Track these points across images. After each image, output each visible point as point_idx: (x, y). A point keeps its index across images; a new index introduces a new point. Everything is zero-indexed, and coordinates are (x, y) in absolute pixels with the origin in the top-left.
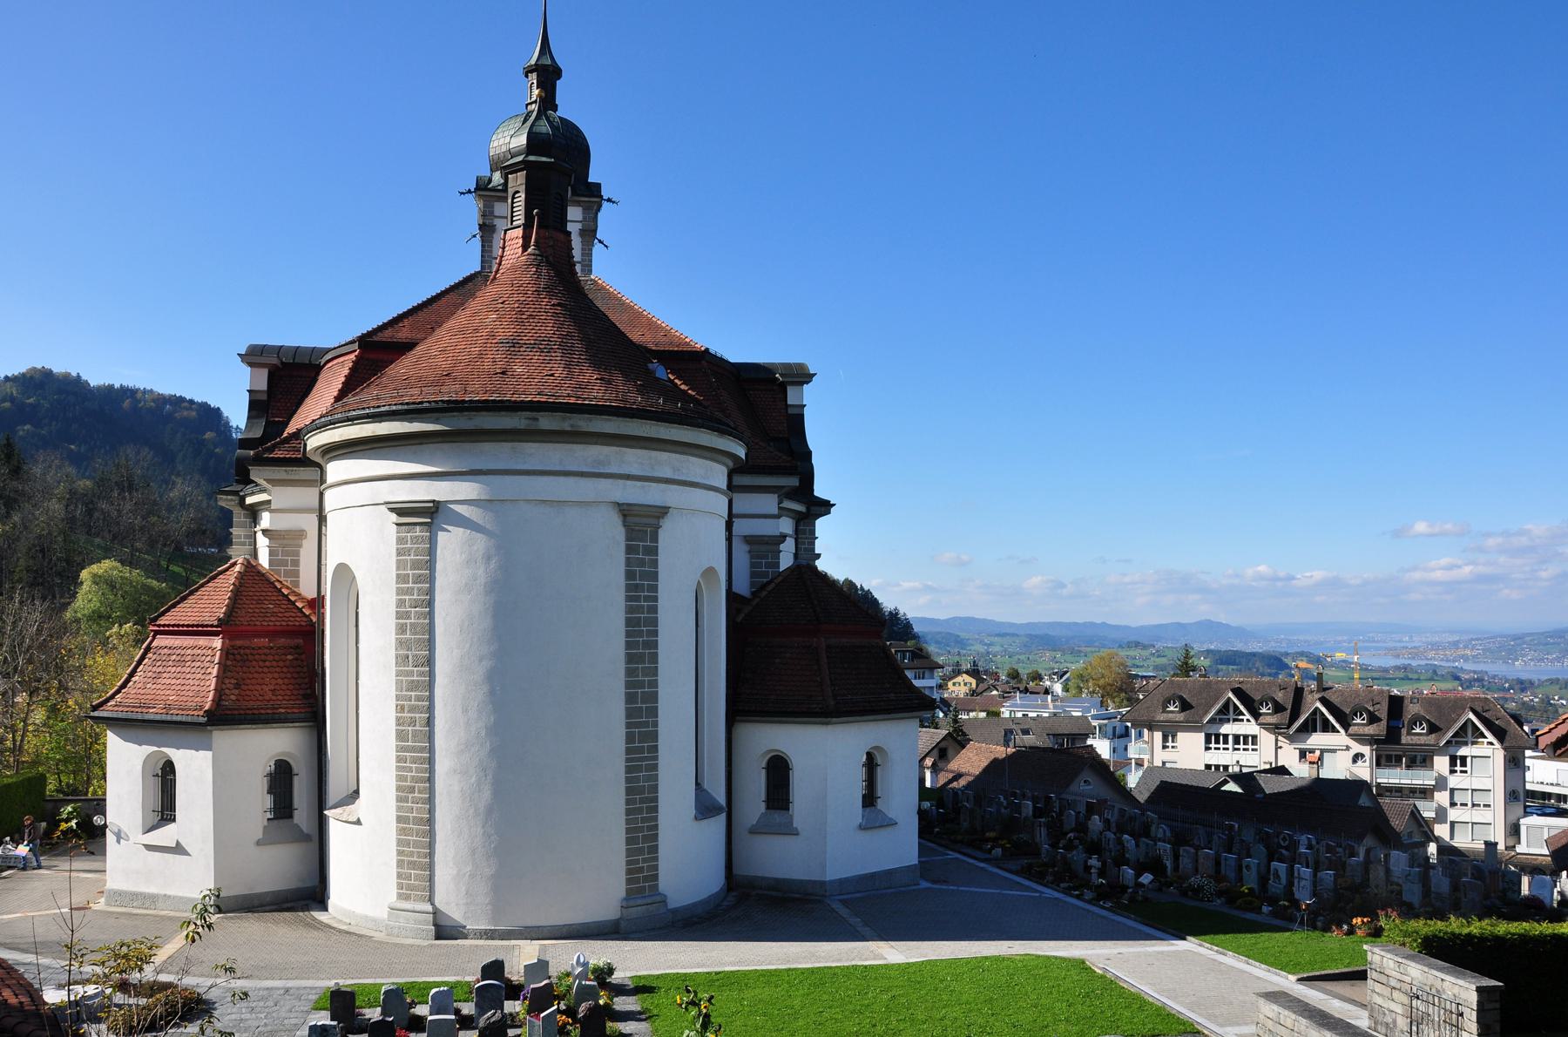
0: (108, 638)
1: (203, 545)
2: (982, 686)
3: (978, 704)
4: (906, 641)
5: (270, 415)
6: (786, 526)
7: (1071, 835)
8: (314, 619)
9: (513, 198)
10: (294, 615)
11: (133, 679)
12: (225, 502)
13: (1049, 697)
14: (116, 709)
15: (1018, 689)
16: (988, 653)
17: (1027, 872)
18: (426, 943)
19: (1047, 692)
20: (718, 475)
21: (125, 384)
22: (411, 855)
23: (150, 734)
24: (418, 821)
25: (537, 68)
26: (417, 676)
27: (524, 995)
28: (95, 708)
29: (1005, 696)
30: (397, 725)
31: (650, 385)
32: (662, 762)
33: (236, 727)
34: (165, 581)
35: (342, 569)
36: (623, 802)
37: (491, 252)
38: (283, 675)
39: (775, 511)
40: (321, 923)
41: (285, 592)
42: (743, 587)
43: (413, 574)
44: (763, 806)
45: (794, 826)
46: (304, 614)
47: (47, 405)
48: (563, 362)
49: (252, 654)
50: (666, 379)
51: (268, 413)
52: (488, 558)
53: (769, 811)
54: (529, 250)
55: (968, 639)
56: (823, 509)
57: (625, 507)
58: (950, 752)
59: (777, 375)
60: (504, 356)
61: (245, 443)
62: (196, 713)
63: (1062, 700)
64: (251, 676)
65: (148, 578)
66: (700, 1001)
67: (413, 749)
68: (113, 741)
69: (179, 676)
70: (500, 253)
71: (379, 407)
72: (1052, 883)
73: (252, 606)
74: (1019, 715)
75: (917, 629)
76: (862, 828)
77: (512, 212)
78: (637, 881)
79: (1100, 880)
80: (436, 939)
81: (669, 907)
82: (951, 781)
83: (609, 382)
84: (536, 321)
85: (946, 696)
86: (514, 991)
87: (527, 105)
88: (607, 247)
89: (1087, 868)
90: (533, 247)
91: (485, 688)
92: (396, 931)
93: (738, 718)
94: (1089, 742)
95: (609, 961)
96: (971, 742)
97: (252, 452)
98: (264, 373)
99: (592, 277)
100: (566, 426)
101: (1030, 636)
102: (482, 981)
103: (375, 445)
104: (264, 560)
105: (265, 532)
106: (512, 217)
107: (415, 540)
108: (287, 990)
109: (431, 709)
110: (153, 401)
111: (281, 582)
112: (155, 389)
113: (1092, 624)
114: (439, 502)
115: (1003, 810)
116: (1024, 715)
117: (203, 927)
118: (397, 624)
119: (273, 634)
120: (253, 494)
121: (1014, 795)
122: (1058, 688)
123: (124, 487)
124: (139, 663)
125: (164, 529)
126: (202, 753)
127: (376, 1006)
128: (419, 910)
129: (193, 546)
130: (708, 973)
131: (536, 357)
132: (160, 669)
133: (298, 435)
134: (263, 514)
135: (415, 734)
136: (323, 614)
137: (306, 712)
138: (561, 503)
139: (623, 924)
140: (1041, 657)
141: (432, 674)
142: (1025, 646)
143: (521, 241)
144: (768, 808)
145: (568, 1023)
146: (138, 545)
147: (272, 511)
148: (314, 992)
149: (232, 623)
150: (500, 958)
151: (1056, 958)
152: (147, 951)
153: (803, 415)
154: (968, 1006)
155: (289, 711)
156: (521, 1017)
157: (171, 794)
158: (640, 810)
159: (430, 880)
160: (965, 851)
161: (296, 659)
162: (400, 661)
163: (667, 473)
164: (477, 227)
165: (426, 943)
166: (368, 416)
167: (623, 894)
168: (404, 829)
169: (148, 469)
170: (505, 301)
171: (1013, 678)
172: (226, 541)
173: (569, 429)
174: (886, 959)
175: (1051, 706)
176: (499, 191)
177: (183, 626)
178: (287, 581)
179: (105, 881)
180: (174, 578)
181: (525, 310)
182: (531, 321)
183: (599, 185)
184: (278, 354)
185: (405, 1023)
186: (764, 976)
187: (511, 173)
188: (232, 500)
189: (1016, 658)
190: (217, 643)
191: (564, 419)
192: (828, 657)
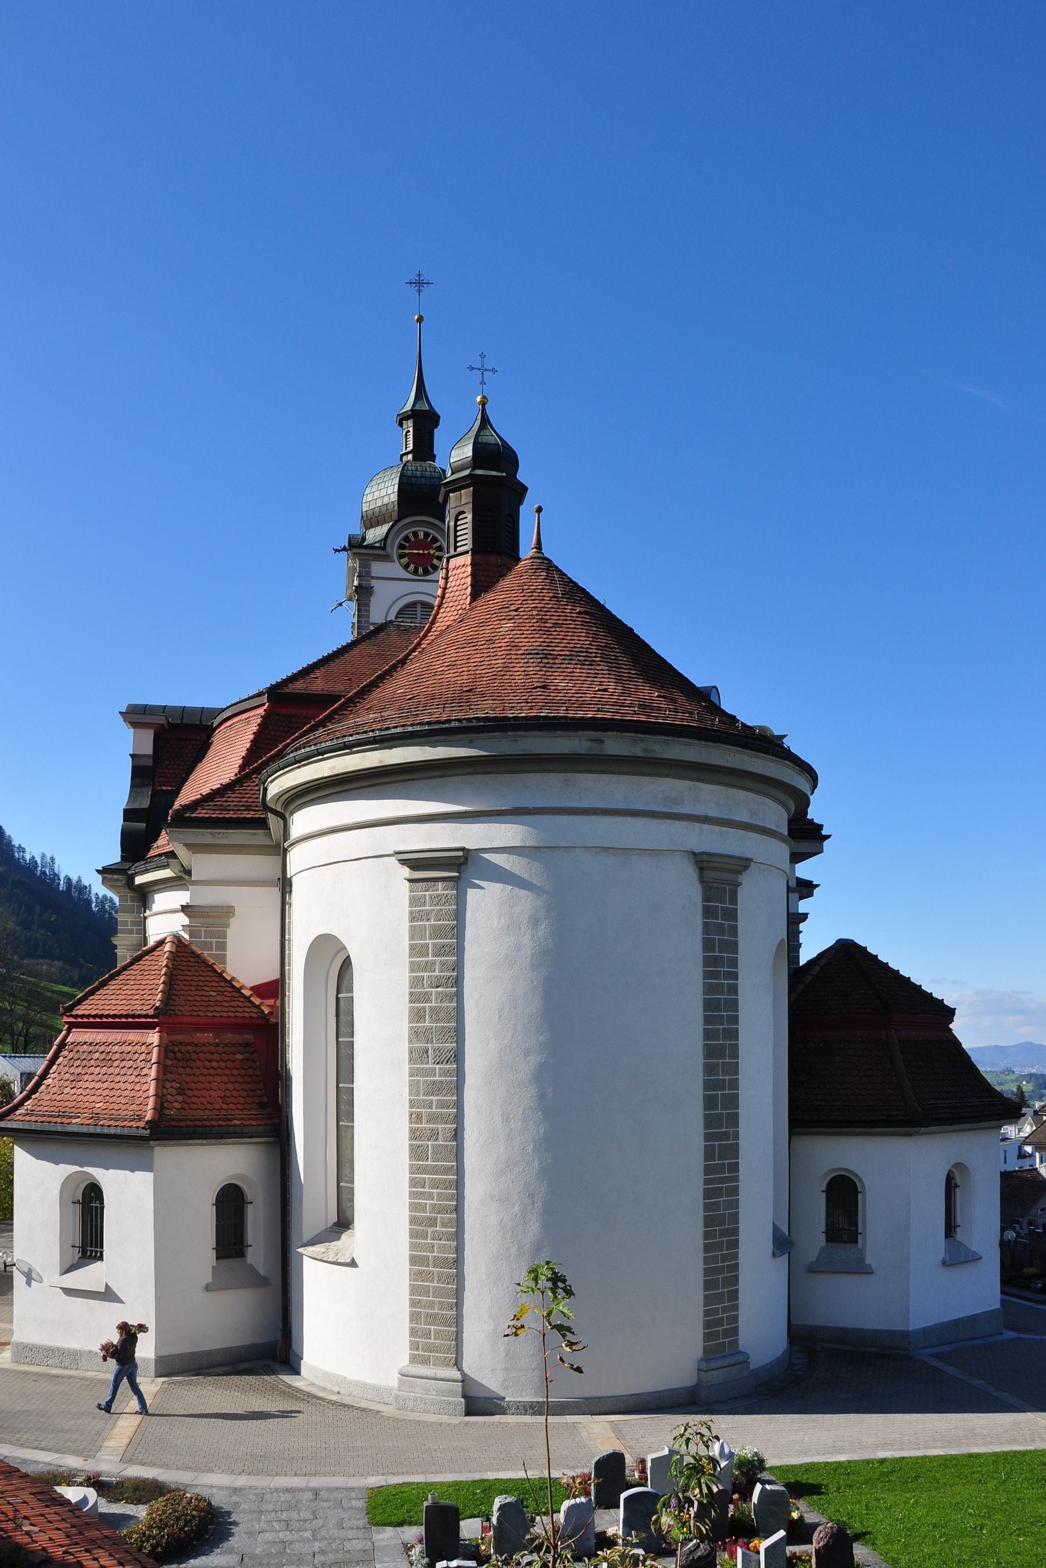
9: (457, 520)
11: (45, 1082)
14: (28, 1118)
22: (431, 1305)
30: (411, 1139)
43: (434, 945)
45: (867, 1262)
46: (254, 1003)
51: (154, 781)
52: (535, 922)
53: (830, 1244)
57: (705, 857)
62: (134, 1124)
67: (434, 1170)
68: (22, 1158)
69: (105, 1078)
71: (387, 729)
80: (466, 1415)
91: (533, 1091)
92: (410, 1404)
95: (755, 1450)
98: (149, 735)
100: (638, 751)
103: (376, 781)
107: (437, 900)
109: (459, 1118)
118: (411, 1010)
120: (146, 871)
126: (139, 1175)
132: (80, 1070)
135: (437, 1150)
137: (265, 1125)
144: (828, 1240)
149: (172, 1012)
157: (96, 1226)
159: (456, 1339)
161: (247, 1059)
165: (445, 1419)
167: (699, 1353)
168: (421, 1273)
170: (518, 608)
173: (640, 754)
177: (107, 1016)
179: (11, 1331)
187: (453, 491)
188: (118, 880)
190: (153, 1037)
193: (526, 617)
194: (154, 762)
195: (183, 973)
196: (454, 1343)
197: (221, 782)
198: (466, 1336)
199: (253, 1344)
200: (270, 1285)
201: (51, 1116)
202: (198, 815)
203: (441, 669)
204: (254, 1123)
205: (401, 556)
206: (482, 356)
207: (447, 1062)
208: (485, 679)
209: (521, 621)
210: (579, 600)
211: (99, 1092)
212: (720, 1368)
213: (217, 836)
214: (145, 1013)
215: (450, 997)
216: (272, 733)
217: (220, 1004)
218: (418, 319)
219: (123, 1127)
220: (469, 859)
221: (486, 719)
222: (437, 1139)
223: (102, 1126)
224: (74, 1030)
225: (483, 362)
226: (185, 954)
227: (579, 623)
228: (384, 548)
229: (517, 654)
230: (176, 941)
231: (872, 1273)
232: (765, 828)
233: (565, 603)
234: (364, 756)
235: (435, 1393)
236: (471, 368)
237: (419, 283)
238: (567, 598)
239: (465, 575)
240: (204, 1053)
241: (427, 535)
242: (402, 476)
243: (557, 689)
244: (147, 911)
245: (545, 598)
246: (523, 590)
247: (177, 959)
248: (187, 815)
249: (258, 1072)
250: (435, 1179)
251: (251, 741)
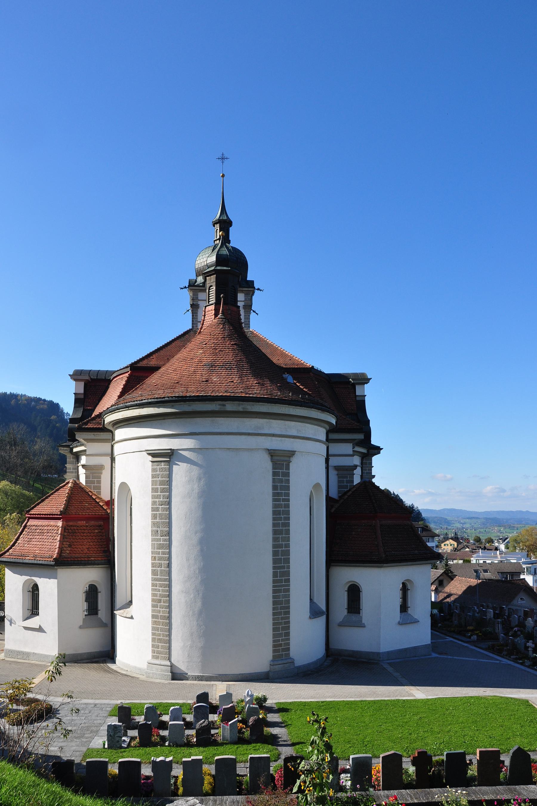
0: (5, 521)
1: (51, 474)
2: (460, 546)
3: (458, 556)
4: (418, 522)
5: (85, 406)
6: (357, 460)
7: (516, 629)
8: (109, 511)
9: (209, 289)
11: (18, 542)
12: (63, 451)
13: (498, 552)
14: (9, 557)
15: (480, 547)
16: (463, 528)
17: (491, 649)
18: (167, 682)
19: (496, 549)
20: (321, 433)
21: (12, 392)
22: (159, 635)
24: (163, 618)
26: (163, 541)
27: (219, 712)
29: (473, 551)
31: (285, 386)
32: (292, 588)
33: (69, 567)
34: (32, 491)
35: (123, 485)
36: (271, 609)
37: (197, 318)
38: (93, 540)
39: (351, 453)
40: (112, 670)
41: (94, 497)
42: (334, 494)
43: (161, 488)
44: (346, 612)
45: (363, 622)
46: (104, 509)
48: (238, 375)
49: (77, 530)
50: (293, 383)
51: (84, 405)
52: (200, 479)
53: (349, 614)
54: (219, 316)
55: (451, 521)
56: (376, 451)
57: (272, 451)
58: (445, 582)
59: (350, 380)
60: (207, 372)
61: (73, 420)
62: (49, 560)
63: (505, 553)
64: (77, 541)
65: (23, 490)
66: (320, 720)
67: (160, 580)
70: (203, 319)
71: (142, 400)
72: (506, 656)
73: (77, 504)
74: (481, 562)
75: (424, 515)
76: (399, 623)
77: (209, 297)
78: (278, 651)
79: (534, 655)
80: (172, 680)
81: (295, 666)
82: (445, 598)
83: (263, 385)
84: (223, 353)
85: (440, 551)
86: (214, 709)
87: (214, 241)
88: (257, 314)
89: (527, 648)
90: (221, 314)
94: (522, 577)
95: (264, 694)
96: (456, 577)
97: (76, 425)
98: (82, 384)
99: (251, 330)
100: (240, 409)
101: (486, 519)
102: (197, 703)
104: (83, 480)
105: (83, 466)
106: (209, 299)
107: (161, 470)
108: (95, 705)
109: (170, 559)
110: (26, 400)
111: (92, 492)
112: (27, 395)
113: (521, 512)
114: (174, 450)
115: (476, 615)
116: (484, 562)
117: (56, 673)
118: (152, 514)
119: (88, 519)
120: (77, 446)
121: (483, 606)
122: (502, 547)
123: (12, 444)
124: (21, 533)
125: (31, 465)
126: (56, 580)
127: (141, 715)
128: (163, 664)
129: (45, 473)
130: (317, 702)
131: (224, 372)
133: (100, 416)
134: (82, 457)
136: (113, 508)
137: (104, 560)
139: (271, 674)
140: (492, 530)
141: (170, 540)
142: (484, 524)
143: (213, 312)
144: (348, 612)
145: (243, 728)
146: (19, 473)
147: (87, 455)
148: (109, 706)
150: (206, 691)
151: (512, 698)
152: (28, 685)
153: (365, 401)
154: (463, 725)
155: (96, 559)
156: (218, 723)
157: (37, 601)
158: (280, 613)
159: (169, 649)
160: (457, 637)
161: (100, 532)
162: (154, 533)
163: (294, 433)
164: (190, 306)
165: (167, 682)
167: (270, 657)
168: (156, 622)
169: (23, 434)
170: (206, 343)
171: (478, 542)
172: (62, 471)
173: (242, 410)
174: (415, 696)
175: (499, 557)
177: (43, 514)
178: (94, 492)
180: (36, 490)
181: (217, 347)
182: (221, 353)
183: (252, 282)
184: (89, 374)
185: (157, 725)
186: (348, 704)
187: (208, 276)
188: (66, 450)
189: (478, 531)
190: (60, 523)
191: (239, 405)
192: (381, 531)
193: (209, 347)
194: (84, 396)
195: (75, 496)
196: (168, 650)
197: (99, 412)
199: (100, 651)
200: (107, 626)
201: (18, 556)
202: (88, 427)
203: (170, 372)
204: (100, 559)
207: (165, 536)
208: (185, 377)
209: (206, 349)
210: (234, 338)
211: (38, 546)
212: (280, 664)
213: (96, 435)
214: (57, 513)
215: (166, 509)
216: (132, 384)
217: (89, 509)
218: (222, 176)
219: (45, 561)
220: (174, 453)
221: (178, 397)
222: (161, 567)
223: (37, 560)
224: (30, 520)
226: (77, 488)
227: (231, 350)
229: (200, 365)
230: (74, 482)
231: (365, 627)
232: (304, 437)
233: (227, 340)
234: (133, 411)
235: (160, 671)
237: (223, 158)
238: (229, 338)
239: (212, 314)
240: (81, 530)
243: (211, 382)
244: (79, 463)
245: (219, 338)
247: (73, 490)
248: (84, 427)
249: (104, 537)
250: (161, 583)
251: (122, 388)
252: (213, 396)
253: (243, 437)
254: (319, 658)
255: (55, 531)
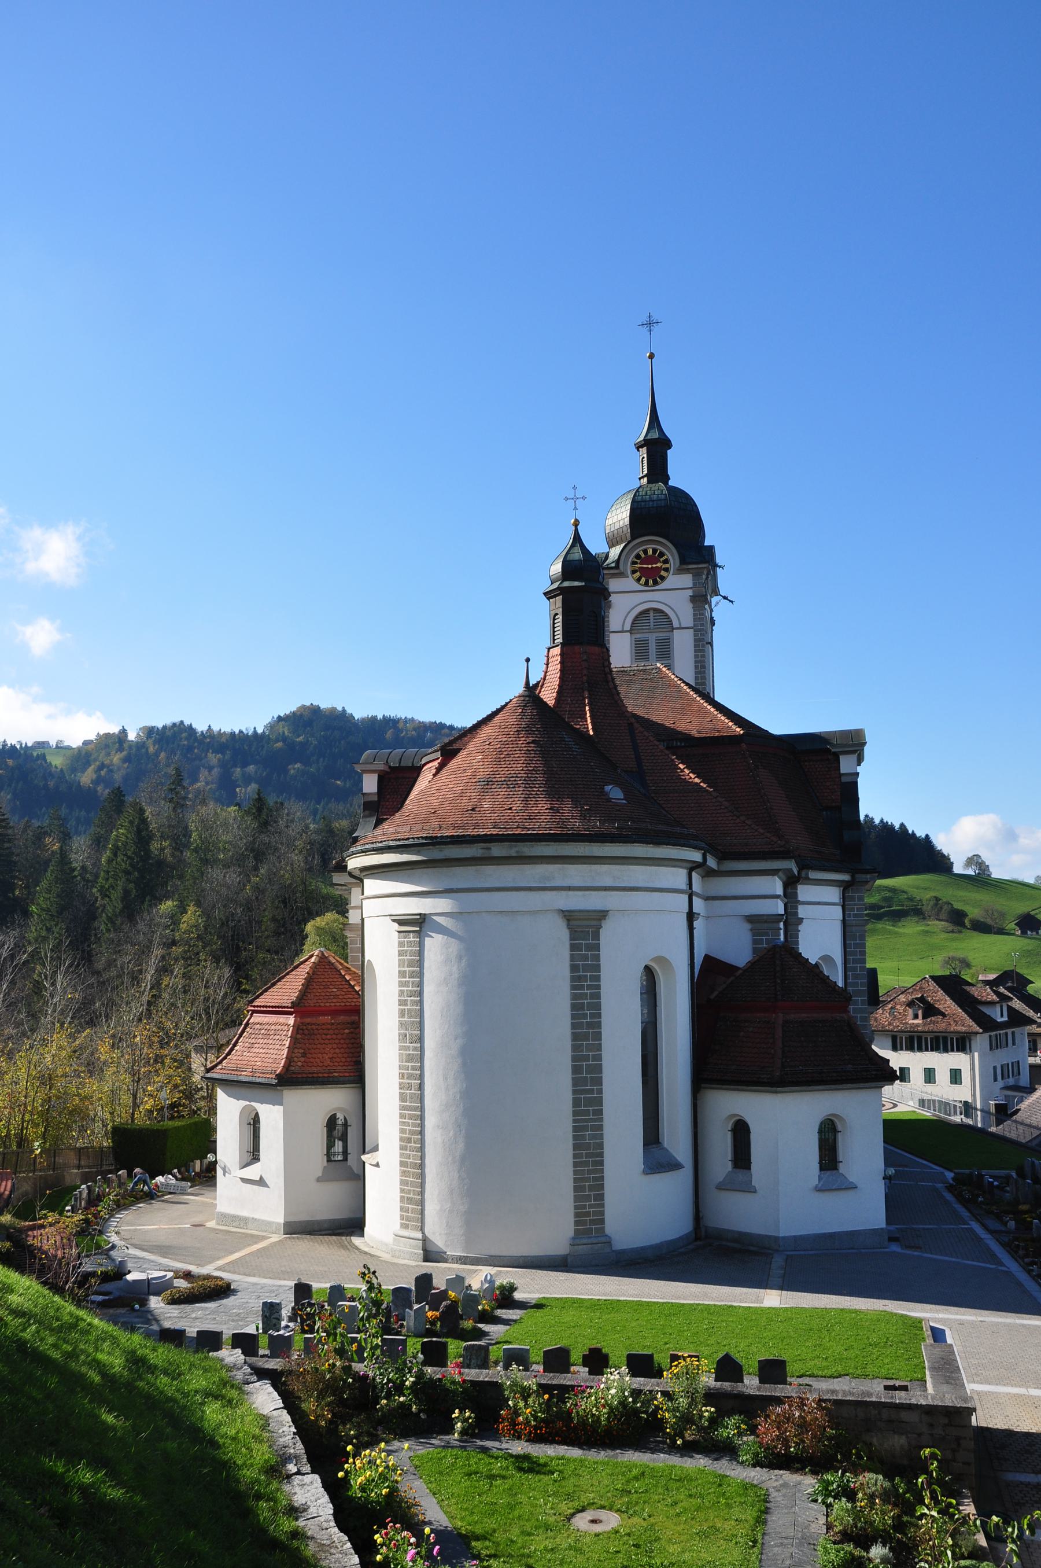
10: (351, 996)
14: (221, 1071)
18: (417, 1263)
21: (387, 714)
22: (409, 1192)
23: (244, 1091)
24: (414, 1166)
25: (647, 443)
28: (208, 1071)
38: (340, 1046)
44: (729, 1166)
47: (315, 742)
52: (460, 958)
62: (270, 1076)
76: (819, 1189)
78: (584, 1223)
88: (732, 602)
93: (703, 1085)
109: (421, 1077)
110: (414, 729)
112: (416, 718)
132: (253, 1041)
138: (514, 913)
141: (422, 1049)
143: (559, 658)
158: (587, 1164)
161: (352, 1033)
163: (608, 882)
166: (373, 850)
168: (404, 1172)
176: (612, 568)
177: (269, 1007)
183: (711, 548)
190: (291, 1020)
198: (426, 1212)
204: (347, 1074)
205: (634, 572)
206: (575, 488)
221: (426, 838)
225: (575, 493)
228: (617, 567)
236: (566, 499)
241: (654, 551)
242: (633, 502)
246: (500, 726)
252: (473, 836)
253: (522, 894)
254: (669, 1238)
255: (285, 1033)
